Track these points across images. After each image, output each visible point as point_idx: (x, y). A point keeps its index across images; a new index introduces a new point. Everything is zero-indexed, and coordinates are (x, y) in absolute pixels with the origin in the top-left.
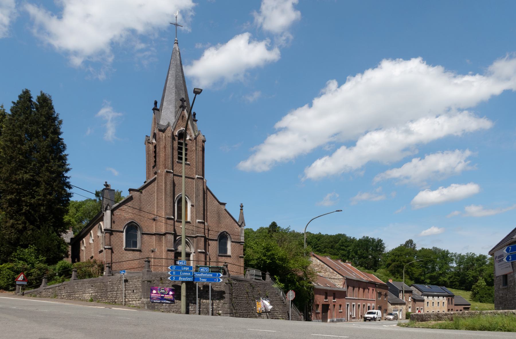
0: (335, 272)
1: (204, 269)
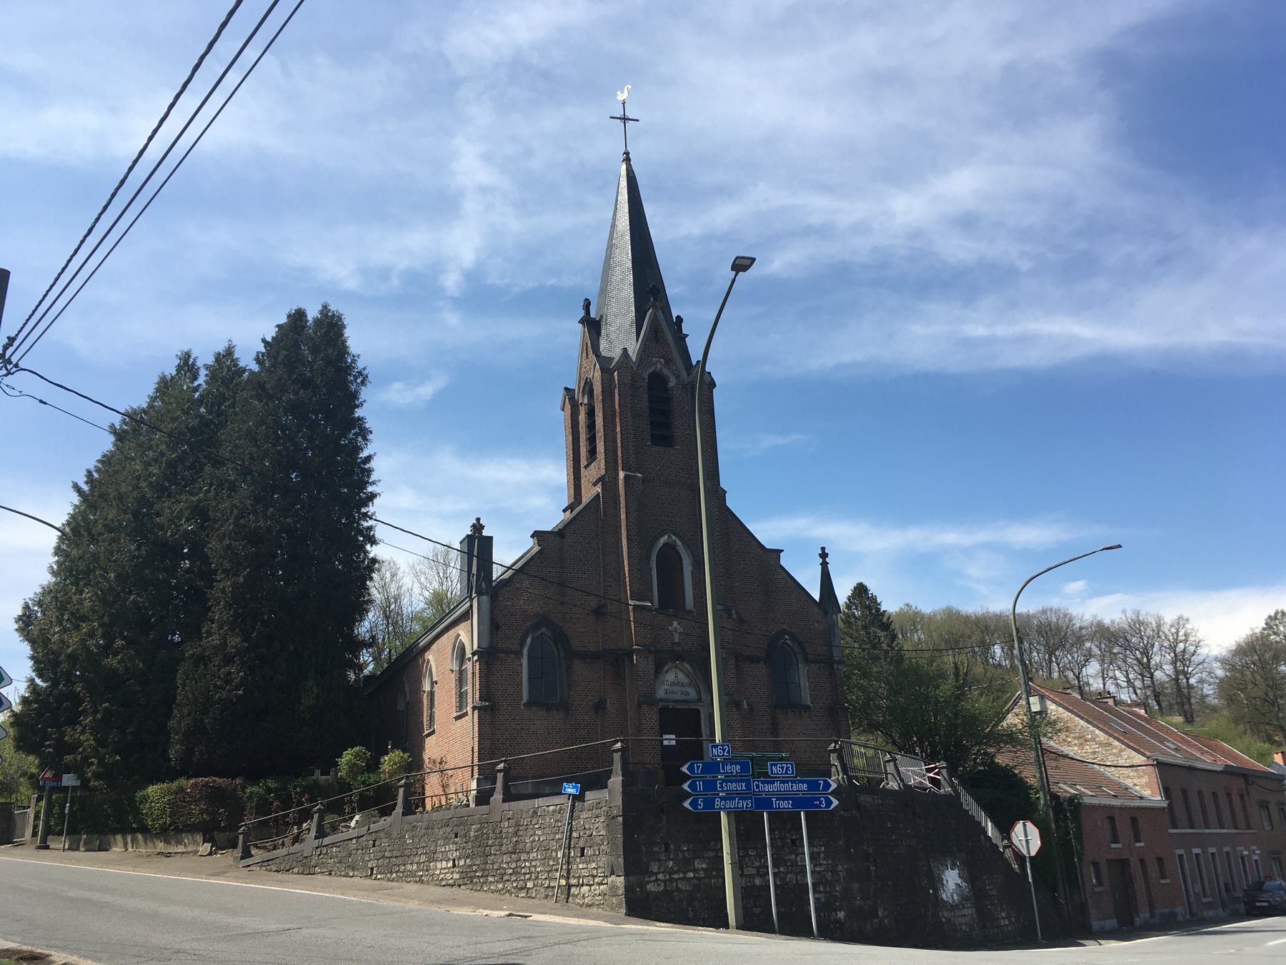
0: (1116, 743)
1: (783, 768)
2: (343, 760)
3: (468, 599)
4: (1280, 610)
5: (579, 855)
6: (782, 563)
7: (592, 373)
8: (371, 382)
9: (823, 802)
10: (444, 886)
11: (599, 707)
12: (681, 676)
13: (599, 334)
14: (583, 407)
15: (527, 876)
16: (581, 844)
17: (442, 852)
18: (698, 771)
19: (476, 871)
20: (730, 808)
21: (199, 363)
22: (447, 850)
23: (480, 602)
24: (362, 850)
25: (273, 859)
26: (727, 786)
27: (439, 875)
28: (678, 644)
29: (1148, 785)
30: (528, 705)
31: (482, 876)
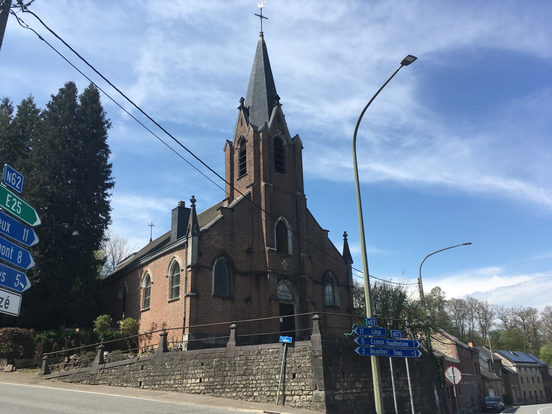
2: (97, 322)
3: (185, 238)
4: (437, 287)
5: (292, 378)
6: (329, 237)
7: (247, 133)
8: (112, 127)
9: (415, 353)
10: (193, 393)
11: (248, 300)
12: (286, 287)
13: (248, 115)
14: (237, 150)
15: (254, 389)
16: (293, 371)
17: (192, 373)
18: (361, 332)
19: (217, 385)
20: (377, 354)
21: (14, 105)
22: (196, 372)
24: (134, 371)
25: (68, 375)
26: (375, 342)
27: (189, 387)
28: (286, 271)
29: (451, 353)
30: (215, 296)
31: (221, 388)
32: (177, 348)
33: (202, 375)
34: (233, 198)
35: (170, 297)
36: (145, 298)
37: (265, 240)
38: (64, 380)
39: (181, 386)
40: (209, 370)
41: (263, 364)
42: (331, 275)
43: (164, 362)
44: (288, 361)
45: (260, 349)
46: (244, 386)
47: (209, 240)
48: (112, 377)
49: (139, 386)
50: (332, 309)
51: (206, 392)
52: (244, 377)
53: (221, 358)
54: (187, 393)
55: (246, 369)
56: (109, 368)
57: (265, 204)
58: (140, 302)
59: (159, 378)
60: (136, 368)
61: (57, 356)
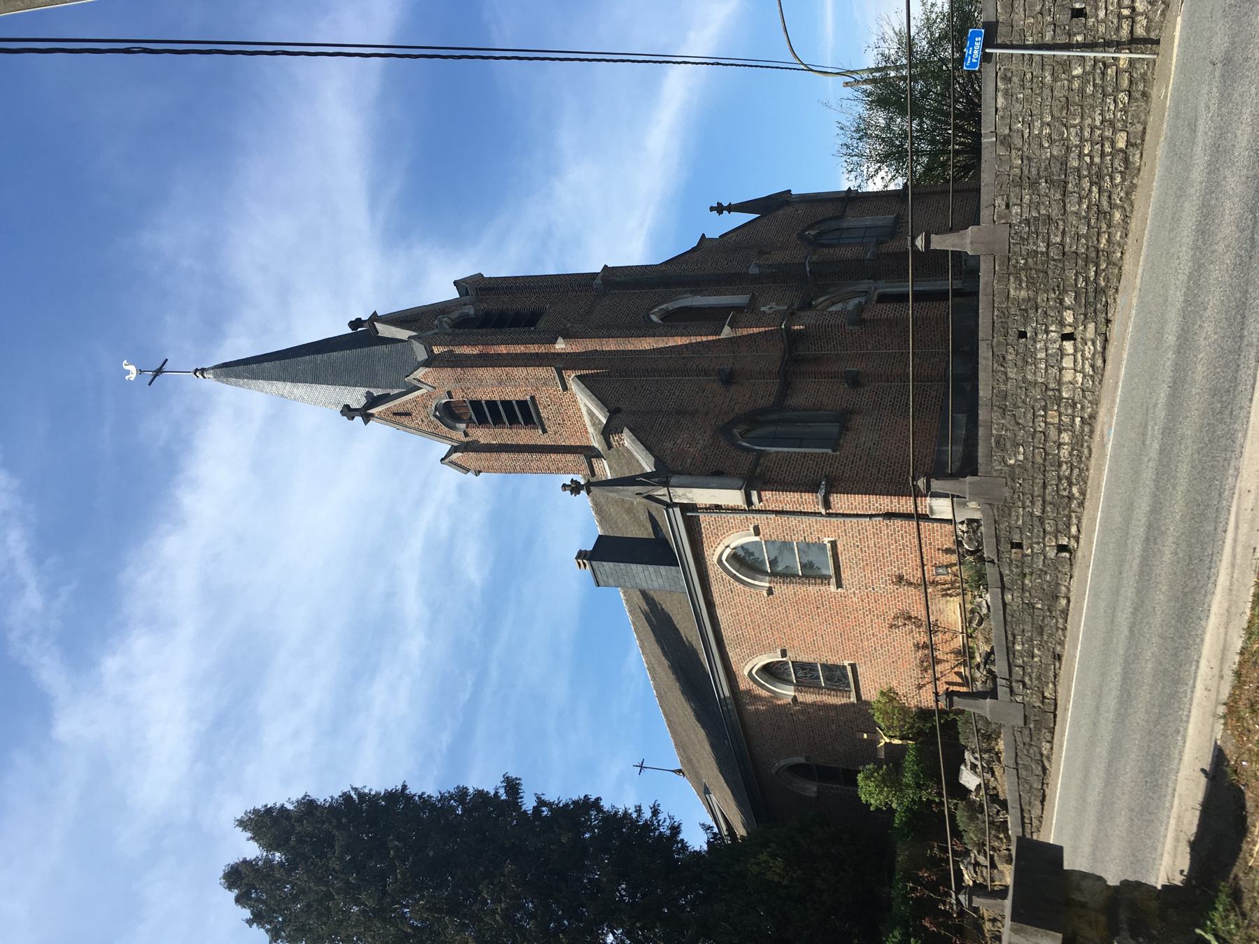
3: (670, 510)
10: (1104, 361)
11: (855, 381)
14: (470, 431)
15: (1108, 149)
16: (1064, 17)
19: (1086, 280)
23: (678, 484)
25: (1022, 810)
27: (1084, 377)
32: (967, 532)
33: (1053, 334)
34: (592, 448)
35: (826, 582)
36: (823, 688)
37: (704, 339)
38: (1034, 825)
39: (1079, 406)
40: (1040, 311)
41: (1038, 124)
42: (813, 233)
43: (1006, 468)
44: (1035, 37)
45: (994, 139)
46: (1096, 183)
47: (684, 458)
48: (1036, 651)
49: (1071, 554)
50: (900, 228)
51: (1104, 315)
52: (1070, 185)
53: (1009, 271)
54: (1101, 381)
55: (1046, 182)
56: (1011, 660)
57: (612, 337)
58: (832, 706)
59: (1051, 485)
60: (1017, 567)
61: (963, 921)
